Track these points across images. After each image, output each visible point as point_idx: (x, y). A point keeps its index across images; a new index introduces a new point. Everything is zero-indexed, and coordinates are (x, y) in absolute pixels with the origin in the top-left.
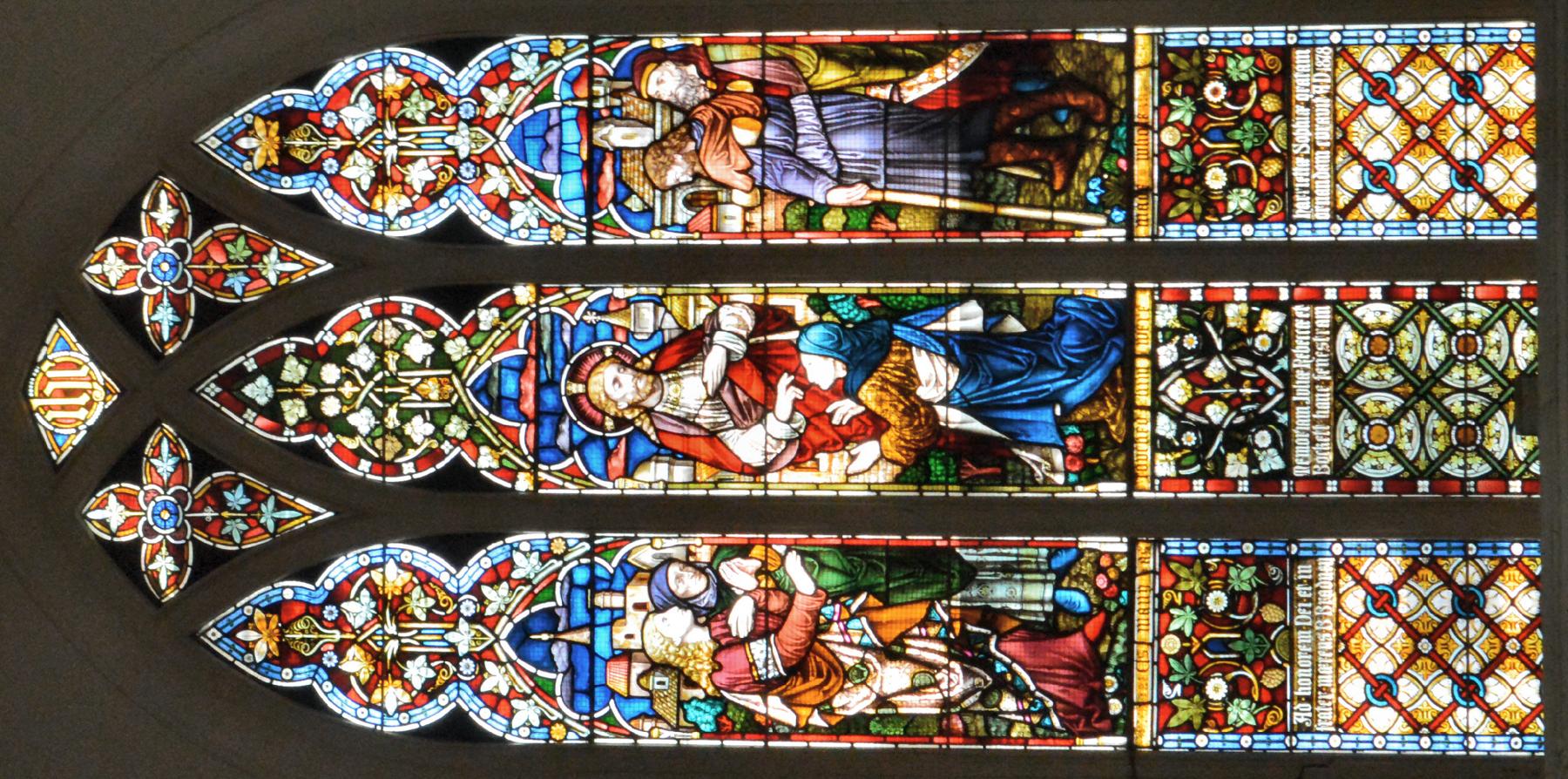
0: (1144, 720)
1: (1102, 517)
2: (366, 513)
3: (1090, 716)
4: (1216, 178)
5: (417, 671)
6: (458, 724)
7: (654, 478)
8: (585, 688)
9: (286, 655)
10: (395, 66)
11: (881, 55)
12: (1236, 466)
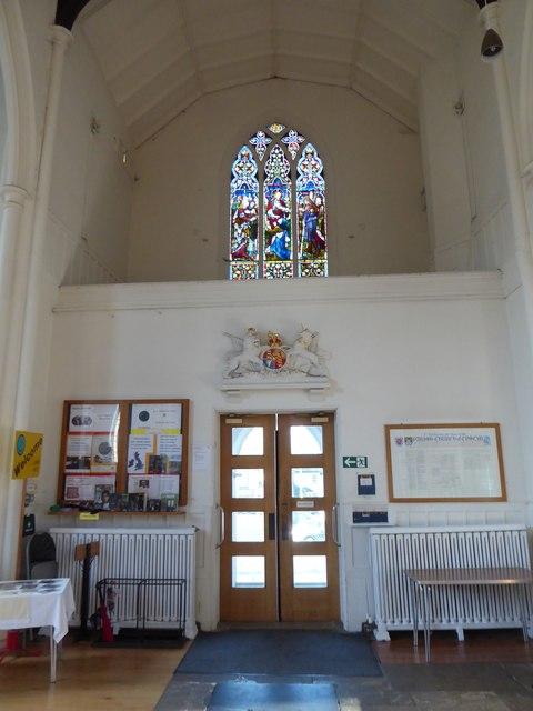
0: (234, 263)
1: (261, 257)
2: (261, 165)
3: (235, 256)
4: (307, 271)
5: (240, 172)
6: (233, 177)
7: (266, 201)
8: (238, 193)
9: (242, 156)
10: (320, 167)
11: (323, 228)
12: (268, 274)
